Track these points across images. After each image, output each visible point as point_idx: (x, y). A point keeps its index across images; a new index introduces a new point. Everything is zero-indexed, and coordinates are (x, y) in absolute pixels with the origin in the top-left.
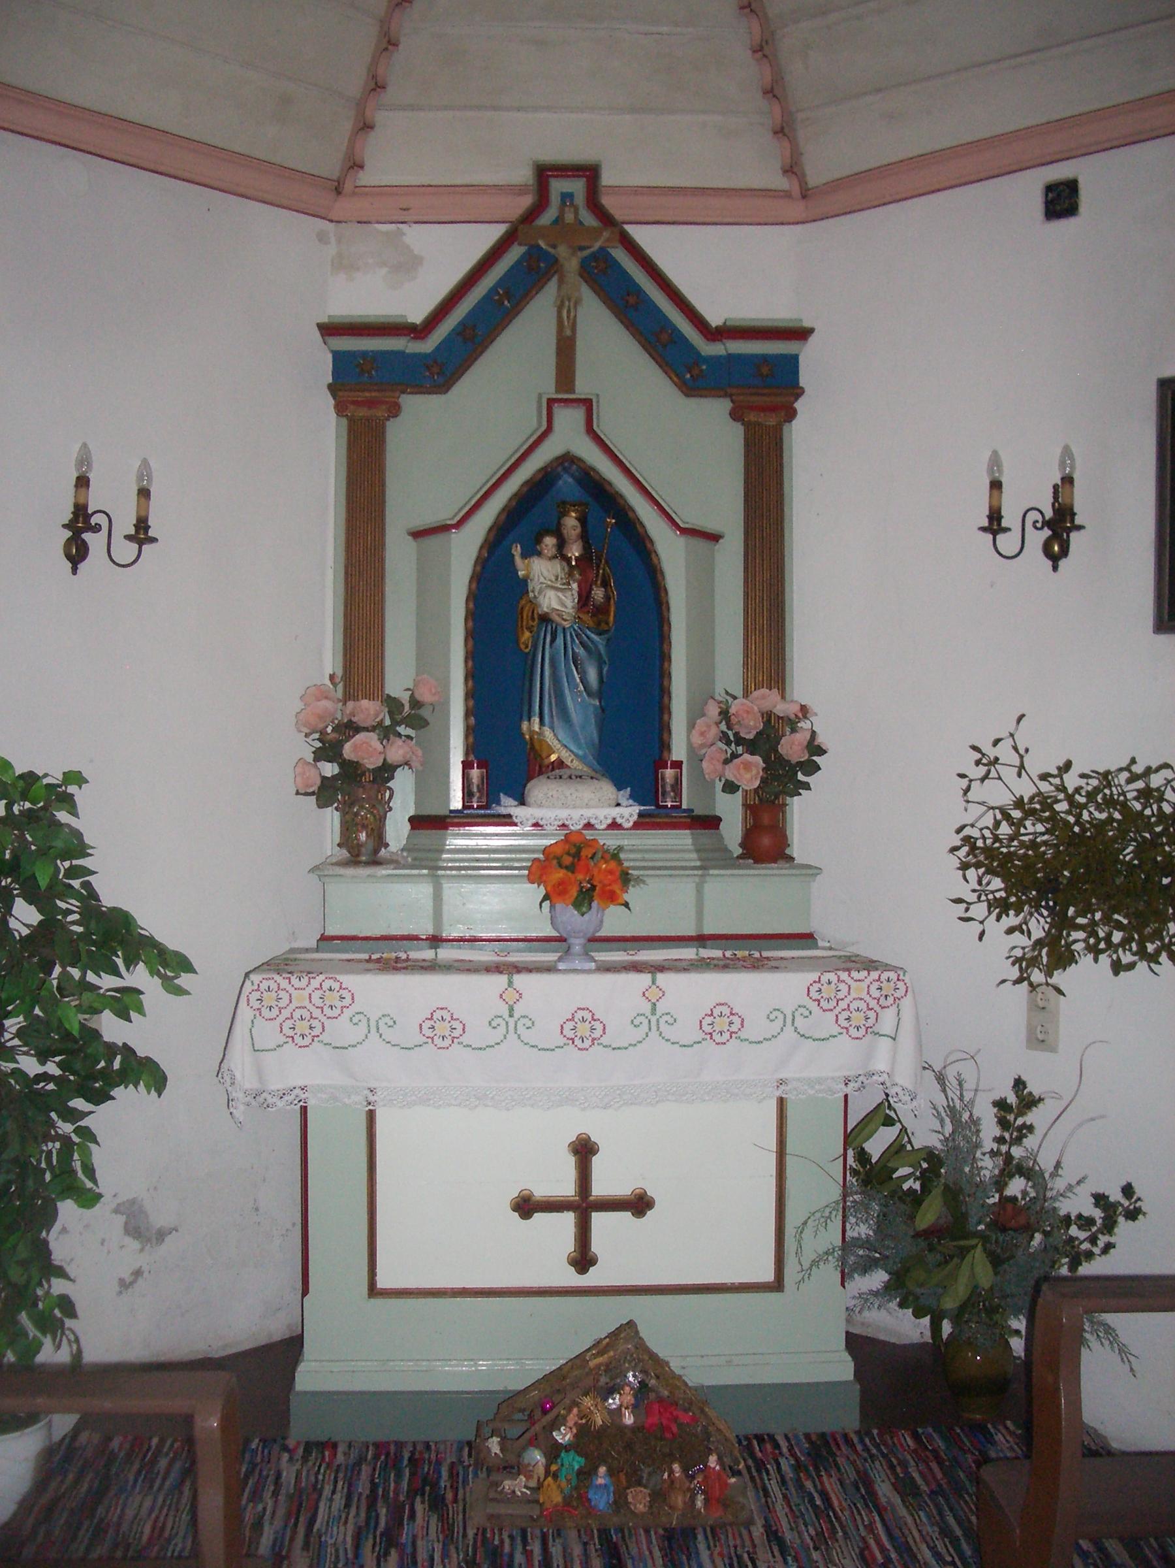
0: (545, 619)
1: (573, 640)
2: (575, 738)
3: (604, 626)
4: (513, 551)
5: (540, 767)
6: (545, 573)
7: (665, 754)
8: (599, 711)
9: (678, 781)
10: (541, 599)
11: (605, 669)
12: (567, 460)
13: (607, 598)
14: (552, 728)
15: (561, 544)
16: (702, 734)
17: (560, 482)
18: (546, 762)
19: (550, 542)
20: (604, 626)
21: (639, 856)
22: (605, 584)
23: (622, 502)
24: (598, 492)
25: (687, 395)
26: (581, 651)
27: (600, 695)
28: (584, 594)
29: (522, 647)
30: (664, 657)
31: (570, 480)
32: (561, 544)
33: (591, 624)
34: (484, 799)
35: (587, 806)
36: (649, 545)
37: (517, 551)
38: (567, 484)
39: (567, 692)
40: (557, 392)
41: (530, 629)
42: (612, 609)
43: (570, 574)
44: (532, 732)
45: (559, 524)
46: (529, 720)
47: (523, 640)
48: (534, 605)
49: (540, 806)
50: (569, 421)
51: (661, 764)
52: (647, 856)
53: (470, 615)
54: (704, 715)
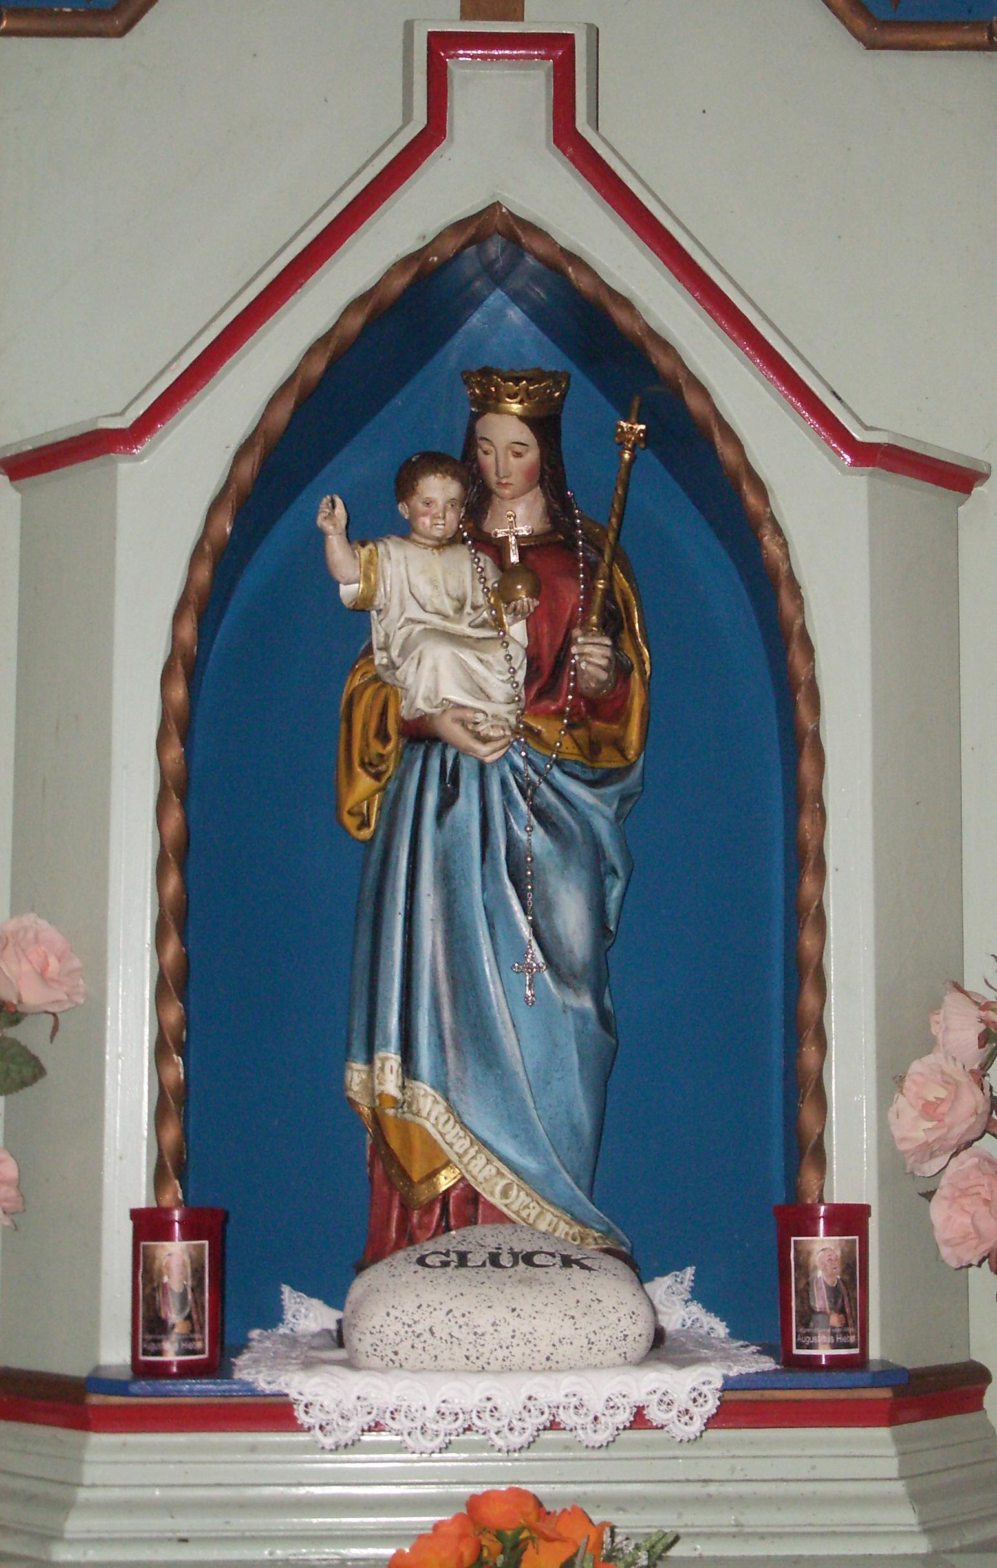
0: (421, 734)
1: (509, 801)
2: (517, 1122)
3: (609, 760)
4: (321, 521)
5: (405, 1210)
6: (424, 589)
7: (809, 1177)
8: (593, 1025)
9: (853, 1272)
10: (407, 672)
11: (615, 891)
12: (495, 239)
13: (620, 670)
14: (442, 1088)
15: (478, 499)
16: (929, 1110)
17: (476, 319)
18: (423, 1194)
19: (438, 490)
20: (609, 760)
21: (726, 1519)
22: (613, 624)
23: (665, 364)
24: (598, 339)
25: (871, 45)
26: (538, 841)
27: (598, 977)
28: (548, 660)
29: (351, 822)
30: (804, 859)
31: (515, 315)
32: (478, 499)
33: (568, 748)
34: (203, 1342)
35: (550, 1366)
36: (752, 500)
37: (333, 518)
38: (502, 325)
39: (488, 969)
40: (465, 16)
41: (372, 767)
42: (637, 704)
43: (503, 594)
44: (378, 1099)
45: (471, 441)
46: (370, 1061)
47: (350, 803)
48: (385, 688)
49: (393, 1364)
50: (499, 103)
51: (796, 1218)
52: (754, 1519)
53: (181, 726)
54: (928, 1045)
